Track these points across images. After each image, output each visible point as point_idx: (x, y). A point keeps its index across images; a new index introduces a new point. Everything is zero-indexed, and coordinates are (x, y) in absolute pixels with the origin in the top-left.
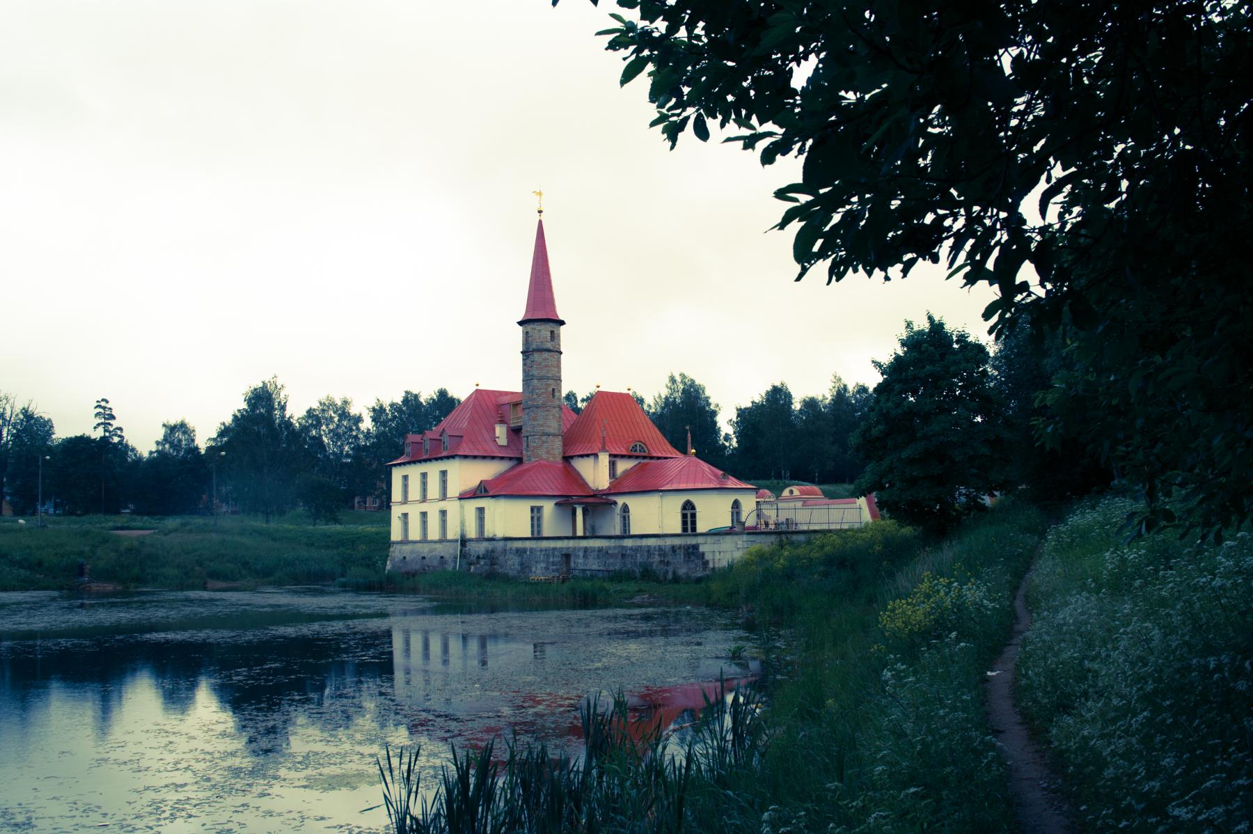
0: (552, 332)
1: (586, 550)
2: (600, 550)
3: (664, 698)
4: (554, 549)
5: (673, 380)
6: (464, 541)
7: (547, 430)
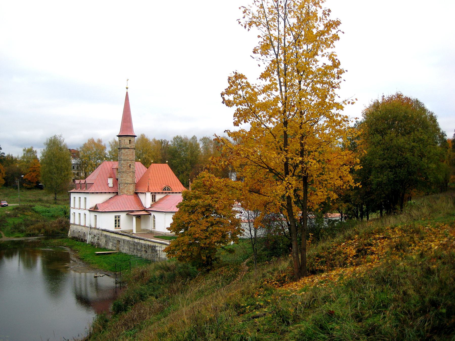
1: (124, 240)
2: (128, 241)
3: (196, 286)
4: (115, 237)
7: (127, 182)
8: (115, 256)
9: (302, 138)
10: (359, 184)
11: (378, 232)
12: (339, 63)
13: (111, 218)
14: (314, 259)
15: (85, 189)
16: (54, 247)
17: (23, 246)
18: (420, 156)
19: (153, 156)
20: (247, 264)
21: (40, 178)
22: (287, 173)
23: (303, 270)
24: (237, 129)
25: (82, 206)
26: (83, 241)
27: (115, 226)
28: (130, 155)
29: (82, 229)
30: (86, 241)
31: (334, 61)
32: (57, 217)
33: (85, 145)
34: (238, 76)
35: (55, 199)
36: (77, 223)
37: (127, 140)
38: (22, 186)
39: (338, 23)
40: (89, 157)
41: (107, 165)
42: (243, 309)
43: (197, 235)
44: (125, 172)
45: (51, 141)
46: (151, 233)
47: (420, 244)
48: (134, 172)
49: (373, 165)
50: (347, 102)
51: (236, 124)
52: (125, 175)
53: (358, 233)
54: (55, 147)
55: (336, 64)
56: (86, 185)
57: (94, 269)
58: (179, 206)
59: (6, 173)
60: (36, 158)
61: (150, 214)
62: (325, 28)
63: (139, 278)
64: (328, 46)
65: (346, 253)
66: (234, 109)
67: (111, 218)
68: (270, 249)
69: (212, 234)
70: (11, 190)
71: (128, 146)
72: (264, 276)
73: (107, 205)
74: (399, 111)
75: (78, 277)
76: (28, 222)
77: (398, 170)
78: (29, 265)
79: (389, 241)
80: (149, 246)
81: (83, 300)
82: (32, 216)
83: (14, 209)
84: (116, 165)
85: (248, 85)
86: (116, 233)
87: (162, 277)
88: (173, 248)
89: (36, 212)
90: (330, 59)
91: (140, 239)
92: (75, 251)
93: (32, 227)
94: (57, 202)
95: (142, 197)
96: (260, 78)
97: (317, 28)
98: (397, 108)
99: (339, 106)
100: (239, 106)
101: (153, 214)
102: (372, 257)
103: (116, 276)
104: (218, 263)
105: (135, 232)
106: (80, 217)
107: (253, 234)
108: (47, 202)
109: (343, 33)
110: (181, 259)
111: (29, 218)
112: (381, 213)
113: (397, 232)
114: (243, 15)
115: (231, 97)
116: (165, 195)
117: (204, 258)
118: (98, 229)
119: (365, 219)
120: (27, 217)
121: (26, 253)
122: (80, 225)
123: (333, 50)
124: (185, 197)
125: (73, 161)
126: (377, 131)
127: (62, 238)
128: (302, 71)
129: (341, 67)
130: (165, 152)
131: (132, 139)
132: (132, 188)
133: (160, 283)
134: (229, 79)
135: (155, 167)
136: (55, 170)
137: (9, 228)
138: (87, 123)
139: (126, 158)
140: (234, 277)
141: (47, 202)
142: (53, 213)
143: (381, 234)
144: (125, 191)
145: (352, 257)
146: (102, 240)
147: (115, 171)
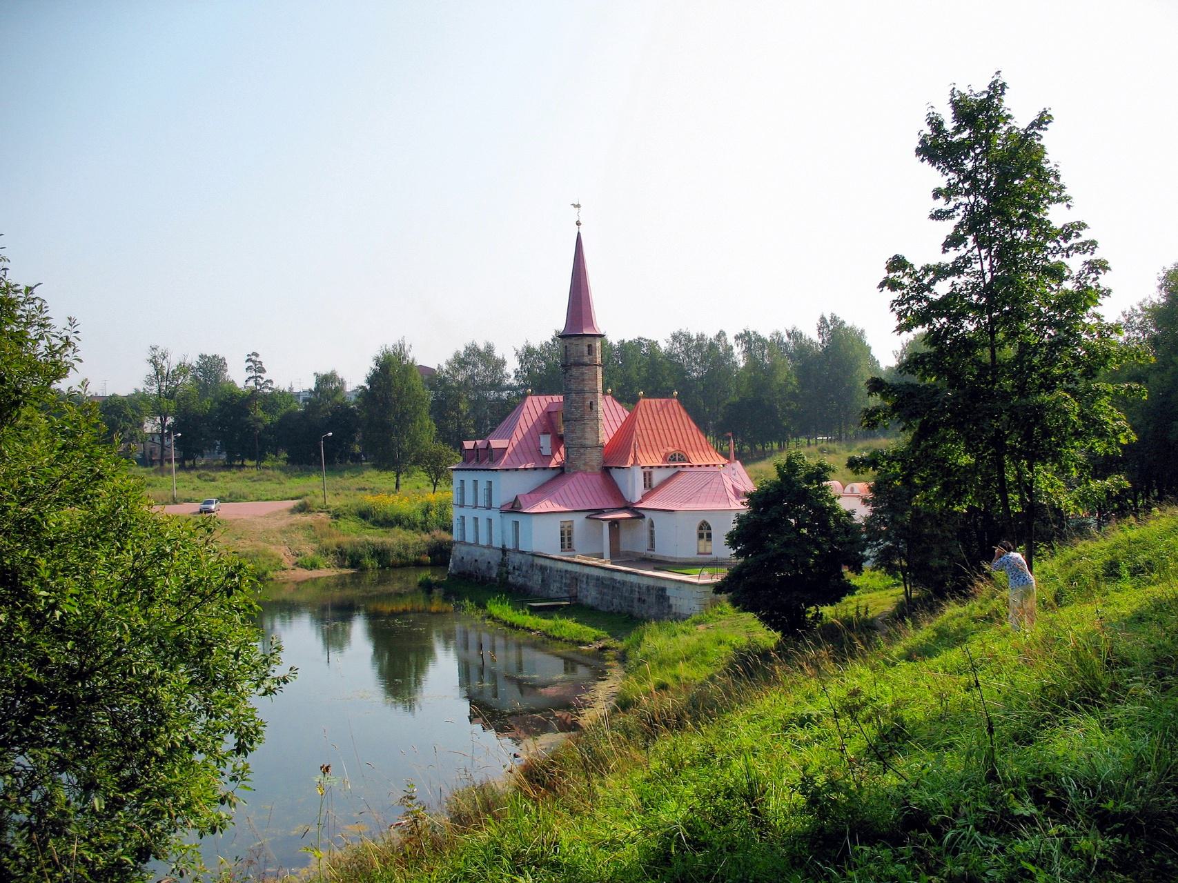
0: (589, 346)
1: (588, 576)
2: (598, 579)
5: (823, 319)
6: (504, 550)
27: (562, 546)
29: (482, 555)
101: (648, 515)
106: (490, 528)
122: (489, 546)
135: (649, 405)
146: (535, 577)
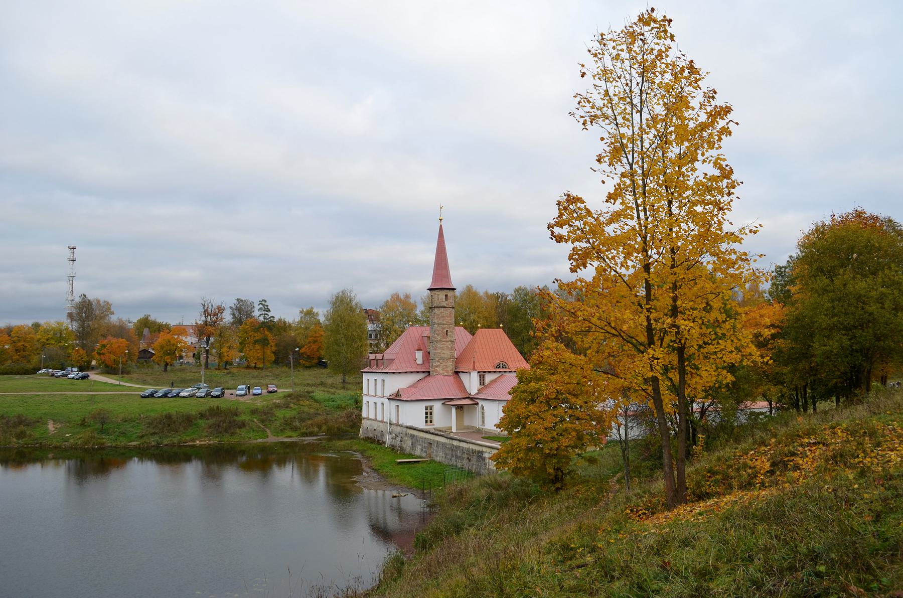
1: (438, 442)
2: (443, 444)
7: (443, 356)
8: (424, 465)
9: (675, 287)
10: (768, 358)
11: (808, 434)
12: (731, 171)
13: (420, 408)
14: (704, 476)
15: (383, 367)
16: (339, 450)
17: (297, 450)
18: (893, 309)
19: (485, 317)
20: (618, 481)
21: (323, 353)
22: (651, 342)
23: (678, 495)
24: (573, 277)
25: (379, 393)
26: (381, 443)
28: (448, 316)
30: (384, 443)
31: (721, 168)
32: (344, 408)
33: (387, 302)
34: (572, 200)
35: (344, 381)
36: (372, 416)
37: (442, 295)
38: (297, 364)
39: (728, 110)
40: (392, 321)
41: (414, 332)
42: (572, 553)
43: (539, 436)
44: (440, 342)
45: (337, 298)
46: (479, 431)
47: (873, 455)
48: (452, 342)
49: (816, 325)
50: (747, 231)
51: (573, 270)
52: (439, 346)
53: (775, 436)
54: (343, 305)
55: (726, 173)
56: (384, 362)
57: (394, 485)
58: (513, 391)
59: (276, 345)
60: (318, 323)
61: (477, 404)
62: (708, 118)
63: (455, 499)
64: (711, 145)
65: (754, 467)
66: (567, 247)
67: (420, 408)
68: (648, 457)
69: (561, 435)
70: (283, 369)
71: (444, 304)
72: (628, 499)
73: (413, 390)
74: (858, 238)
75: (375, 496)
76: (304, 416)
77: (858, 333)
78: (308, 476)
79: (824, 448)
80: (473, 451)
81: (381, 532)
82: (310, 406)
83: (285, 397)
84: (426, 331)
85: (588, 212)
86: (427, 432)
87: (489, 499)
88: (504, 455)
89: (316, 401)
90: (715, 166)
91: (460, 441)
92: (368, 458)
93: (309, 422)
94: (346, 386)
95: (463, 377)
96: (607, 201)
97: (696, 120)
98: (853, 233)
99: (733, 237)
100: (577, 244)
101: (481, 403)
102: (796, 474)
103: (423, 496)
104: (572, 478)
105: (454, 430)
107: (623, 437)
108: (332, 386)
109: (737, 124)
110: (516, 471)
111: (306, 409)
112: (838, 401)
113: (840, 434)
114: (578, 106)
115: (564, 231)
116: (499, 374)
117: (551, 471)
118: (401, 426)
119: (810, 411)
120: (302, 408)
121: (304, 461)
122: (375, 420)
123: (719, 152)
124: (523, 378)
125: (370, 327)
126: (822, 271)
127: (351, 438)
128: (674, 186)
129: (733, 177)
130: (502, 311)
131: (450, 293)
132: (450, 366)
133: (485, 508)
134: (559, 203)
136: (343, 340)
137: (278, 423)
138: (391, 272)
139: (441, 321)
140: (596, 501)
141: (332, 386)
142: (339, 402)
143: (812, 437)
144: (440, 370)
145: (765, 474)
147: (426, 340)
